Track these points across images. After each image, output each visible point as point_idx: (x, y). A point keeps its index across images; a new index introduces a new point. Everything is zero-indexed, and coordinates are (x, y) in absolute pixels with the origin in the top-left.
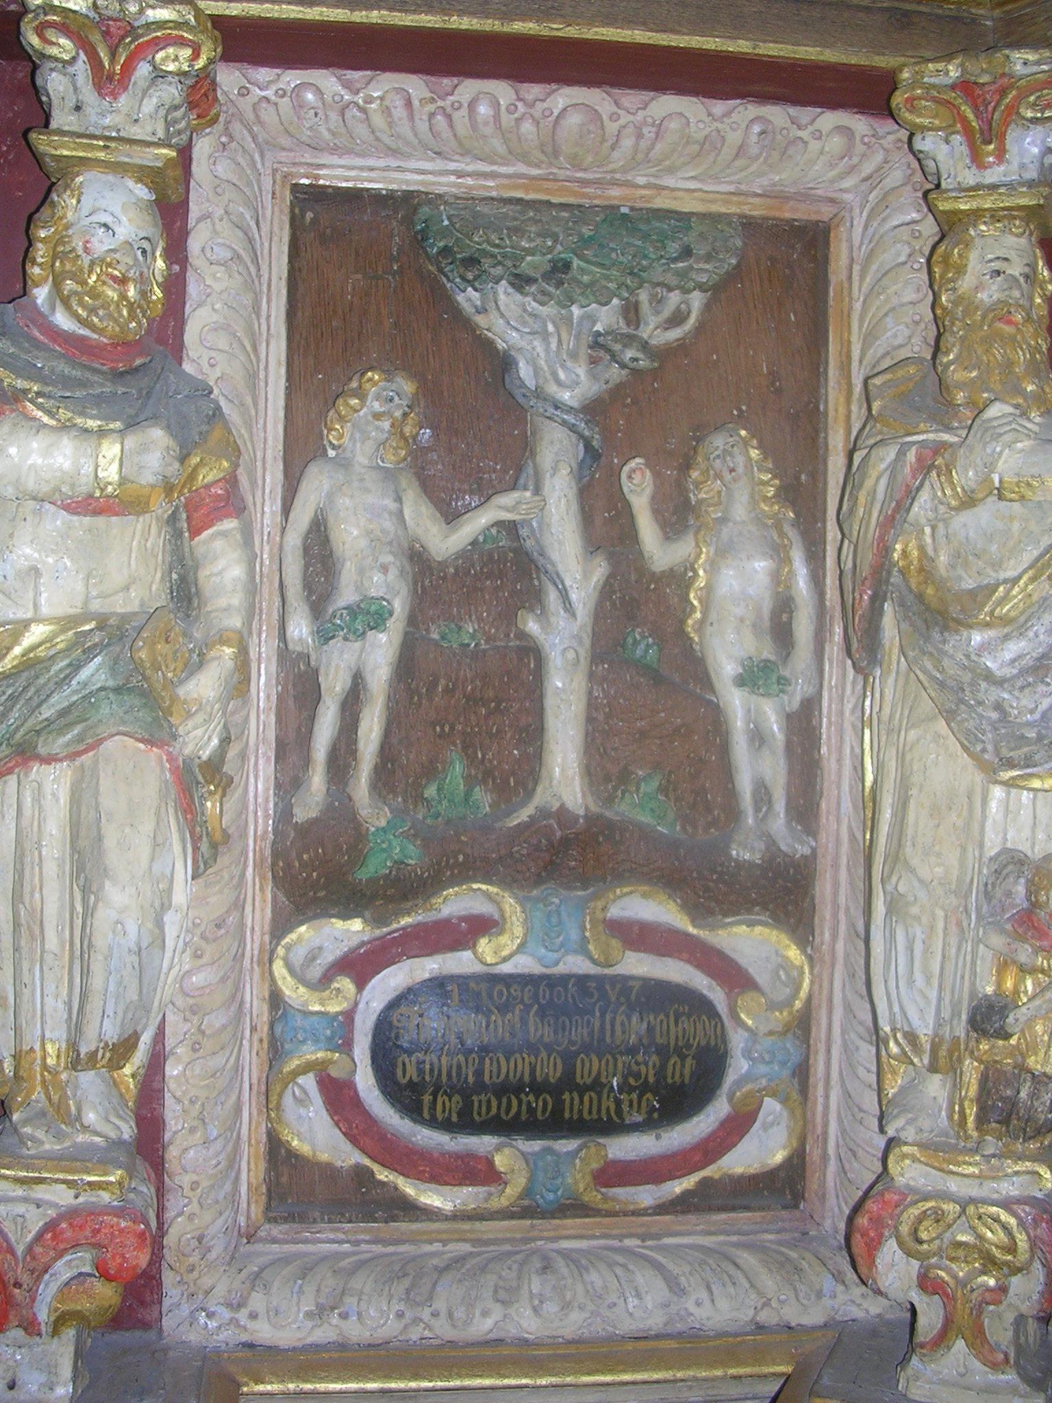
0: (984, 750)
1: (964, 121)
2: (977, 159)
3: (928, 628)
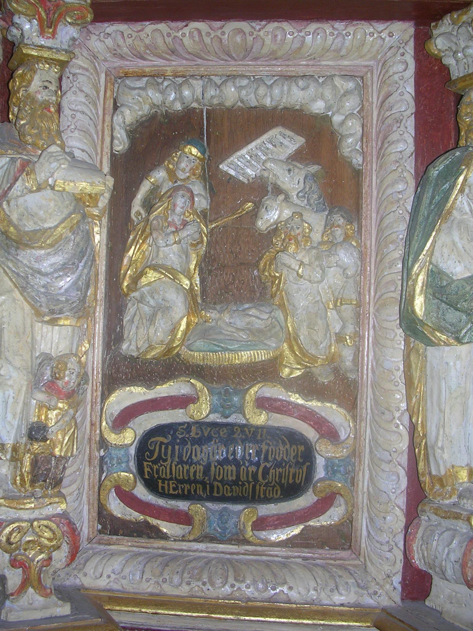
0: (41, 306)
1: (39, 14)
2: (42, 32)
3: (8, 247)
